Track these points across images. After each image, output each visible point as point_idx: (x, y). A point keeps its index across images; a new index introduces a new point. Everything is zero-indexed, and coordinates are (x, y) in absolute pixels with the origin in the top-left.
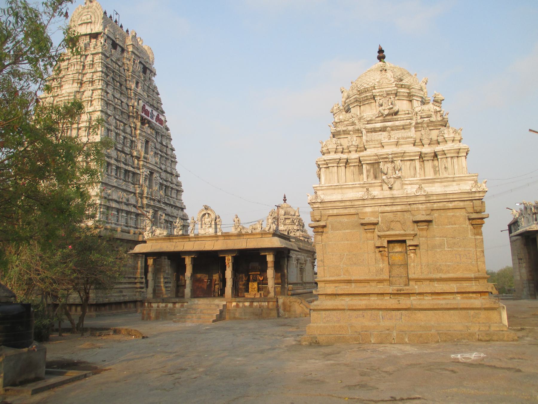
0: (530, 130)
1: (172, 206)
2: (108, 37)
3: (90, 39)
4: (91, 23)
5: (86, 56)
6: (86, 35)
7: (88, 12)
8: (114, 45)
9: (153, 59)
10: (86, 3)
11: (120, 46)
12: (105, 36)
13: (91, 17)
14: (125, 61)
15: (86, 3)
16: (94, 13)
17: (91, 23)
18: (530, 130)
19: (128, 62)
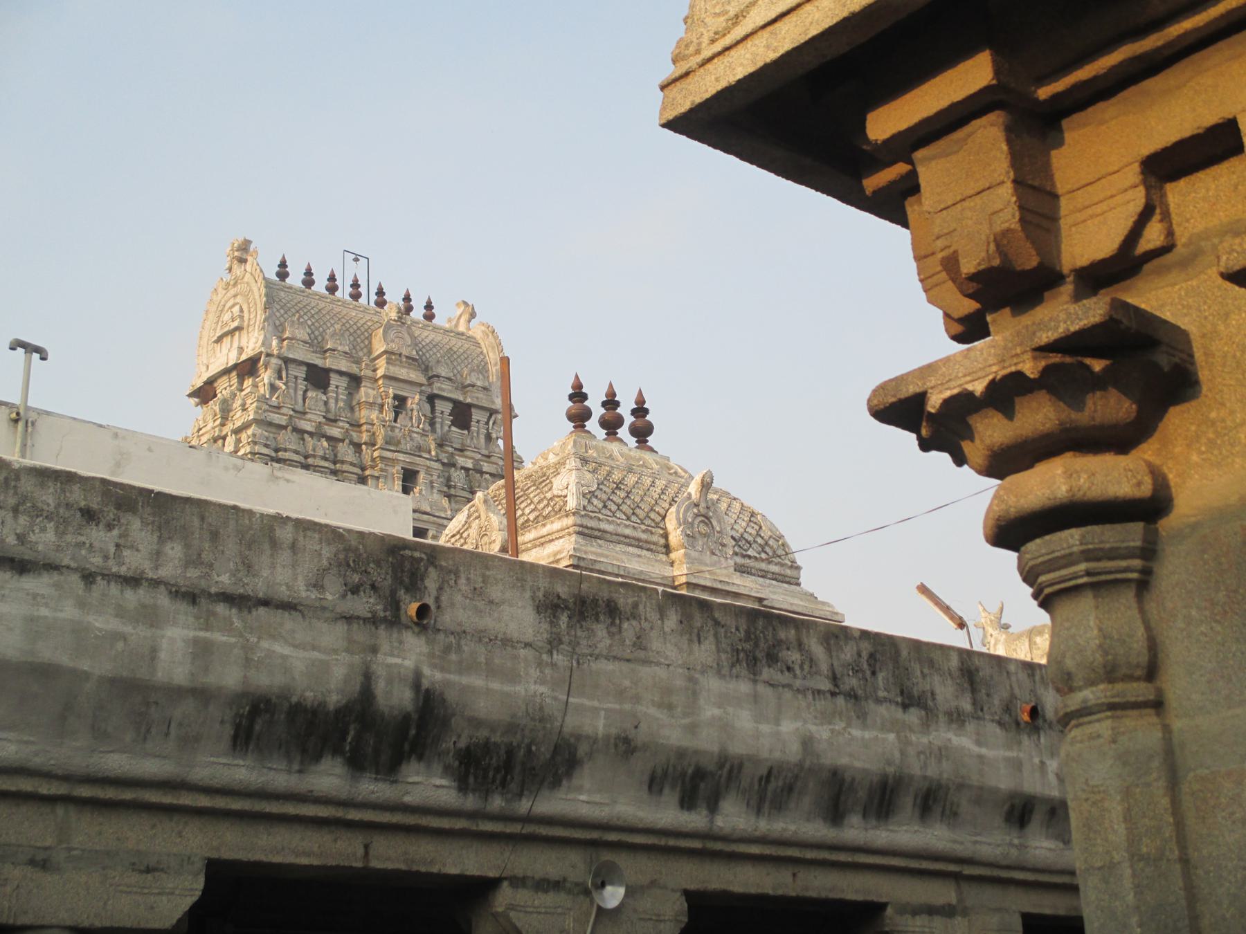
0: (923, 589)
1: (596, 803)
2: (287, 361)
3: (241, 382)
4: (239, 329)
5: (224, 438)
6: (226, 372)
7: (235, 296)
8: (318, 378)
9: (505, 362)
10: (230, 270)
11: (341, 373)
12: (274, 361)
13: (241, 310)
14: (364, 414)
15: (230, 270)
16: (246, 296)
17: (239, 329)
18: (923, 589)
19: (374, 415)
